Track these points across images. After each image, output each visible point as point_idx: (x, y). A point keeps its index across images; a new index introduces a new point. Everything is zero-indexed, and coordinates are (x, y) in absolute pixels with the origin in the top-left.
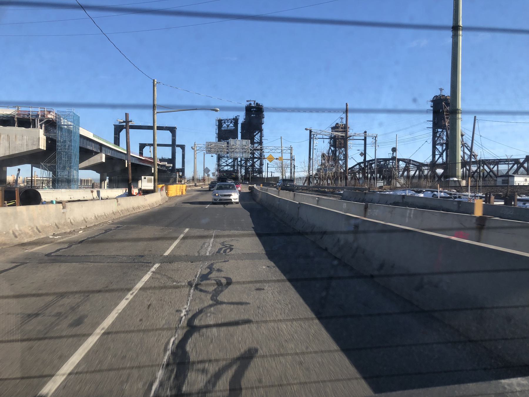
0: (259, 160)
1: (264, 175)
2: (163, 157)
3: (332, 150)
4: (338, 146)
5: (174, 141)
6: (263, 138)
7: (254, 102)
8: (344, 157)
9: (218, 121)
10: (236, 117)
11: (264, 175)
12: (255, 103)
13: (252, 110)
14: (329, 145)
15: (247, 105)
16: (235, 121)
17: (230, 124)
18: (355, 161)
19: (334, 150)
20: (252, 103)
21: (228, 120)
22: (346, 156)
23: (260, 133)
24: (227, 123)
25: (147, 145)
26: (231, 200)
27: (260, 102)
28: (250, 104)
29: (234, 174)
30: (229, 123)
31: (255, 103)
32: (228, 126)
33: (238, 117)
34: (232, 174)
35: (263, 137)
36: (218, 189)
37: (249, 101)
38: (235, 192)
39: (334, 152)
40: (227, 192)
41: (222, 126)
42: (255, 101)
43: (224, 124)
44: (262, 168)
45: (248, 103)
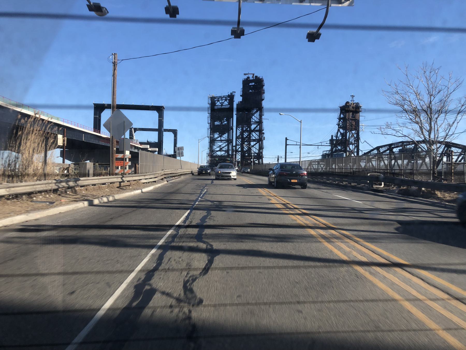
0: (258, 143)
1: (265, 161)
2: (149, 141)
3: (341, 133)
4: (348, 128)
5: (161, 123)
6: (263, 117)
7: (252, 75)
8: (355, 141)
9: (210, 99)
10: (231, 93)
11: (265, 161)
12: (254, 77)
13: (250, 84)
14: (337, 126)
15: (245, 79)
16: (231, 97)
17: (224, 102)
18: (367, 144)
19: (343, 133)
20: (251, 76)
21: (221, 98)
22: (357, 139)
23: (259, 112)
24: (221, 101)
25: (138, 129)
26: (231, 176)
27: (259, 75)
28: (248, 78)
29: (229, 159)
30: (223, 101)
31: (254, 77)
32: (222, 104)
33: (233, 93)
34: (227, 160)
35: (263, 115)
36: (219, 168)
37: (247, 74)
38: (233, 170)
39: (344, 135)
40: (227, 170)
41: (216, 104)
42: (254, 74)
43: (217, 102)
44: (262, 153)
45: (246, 77)
